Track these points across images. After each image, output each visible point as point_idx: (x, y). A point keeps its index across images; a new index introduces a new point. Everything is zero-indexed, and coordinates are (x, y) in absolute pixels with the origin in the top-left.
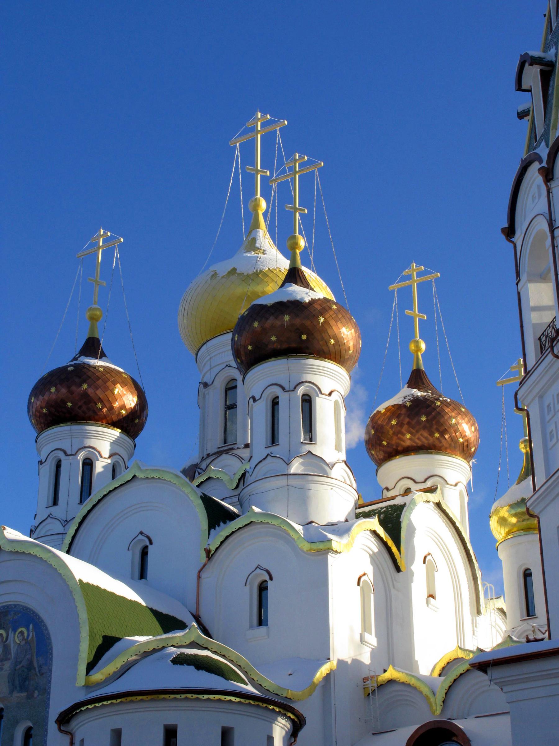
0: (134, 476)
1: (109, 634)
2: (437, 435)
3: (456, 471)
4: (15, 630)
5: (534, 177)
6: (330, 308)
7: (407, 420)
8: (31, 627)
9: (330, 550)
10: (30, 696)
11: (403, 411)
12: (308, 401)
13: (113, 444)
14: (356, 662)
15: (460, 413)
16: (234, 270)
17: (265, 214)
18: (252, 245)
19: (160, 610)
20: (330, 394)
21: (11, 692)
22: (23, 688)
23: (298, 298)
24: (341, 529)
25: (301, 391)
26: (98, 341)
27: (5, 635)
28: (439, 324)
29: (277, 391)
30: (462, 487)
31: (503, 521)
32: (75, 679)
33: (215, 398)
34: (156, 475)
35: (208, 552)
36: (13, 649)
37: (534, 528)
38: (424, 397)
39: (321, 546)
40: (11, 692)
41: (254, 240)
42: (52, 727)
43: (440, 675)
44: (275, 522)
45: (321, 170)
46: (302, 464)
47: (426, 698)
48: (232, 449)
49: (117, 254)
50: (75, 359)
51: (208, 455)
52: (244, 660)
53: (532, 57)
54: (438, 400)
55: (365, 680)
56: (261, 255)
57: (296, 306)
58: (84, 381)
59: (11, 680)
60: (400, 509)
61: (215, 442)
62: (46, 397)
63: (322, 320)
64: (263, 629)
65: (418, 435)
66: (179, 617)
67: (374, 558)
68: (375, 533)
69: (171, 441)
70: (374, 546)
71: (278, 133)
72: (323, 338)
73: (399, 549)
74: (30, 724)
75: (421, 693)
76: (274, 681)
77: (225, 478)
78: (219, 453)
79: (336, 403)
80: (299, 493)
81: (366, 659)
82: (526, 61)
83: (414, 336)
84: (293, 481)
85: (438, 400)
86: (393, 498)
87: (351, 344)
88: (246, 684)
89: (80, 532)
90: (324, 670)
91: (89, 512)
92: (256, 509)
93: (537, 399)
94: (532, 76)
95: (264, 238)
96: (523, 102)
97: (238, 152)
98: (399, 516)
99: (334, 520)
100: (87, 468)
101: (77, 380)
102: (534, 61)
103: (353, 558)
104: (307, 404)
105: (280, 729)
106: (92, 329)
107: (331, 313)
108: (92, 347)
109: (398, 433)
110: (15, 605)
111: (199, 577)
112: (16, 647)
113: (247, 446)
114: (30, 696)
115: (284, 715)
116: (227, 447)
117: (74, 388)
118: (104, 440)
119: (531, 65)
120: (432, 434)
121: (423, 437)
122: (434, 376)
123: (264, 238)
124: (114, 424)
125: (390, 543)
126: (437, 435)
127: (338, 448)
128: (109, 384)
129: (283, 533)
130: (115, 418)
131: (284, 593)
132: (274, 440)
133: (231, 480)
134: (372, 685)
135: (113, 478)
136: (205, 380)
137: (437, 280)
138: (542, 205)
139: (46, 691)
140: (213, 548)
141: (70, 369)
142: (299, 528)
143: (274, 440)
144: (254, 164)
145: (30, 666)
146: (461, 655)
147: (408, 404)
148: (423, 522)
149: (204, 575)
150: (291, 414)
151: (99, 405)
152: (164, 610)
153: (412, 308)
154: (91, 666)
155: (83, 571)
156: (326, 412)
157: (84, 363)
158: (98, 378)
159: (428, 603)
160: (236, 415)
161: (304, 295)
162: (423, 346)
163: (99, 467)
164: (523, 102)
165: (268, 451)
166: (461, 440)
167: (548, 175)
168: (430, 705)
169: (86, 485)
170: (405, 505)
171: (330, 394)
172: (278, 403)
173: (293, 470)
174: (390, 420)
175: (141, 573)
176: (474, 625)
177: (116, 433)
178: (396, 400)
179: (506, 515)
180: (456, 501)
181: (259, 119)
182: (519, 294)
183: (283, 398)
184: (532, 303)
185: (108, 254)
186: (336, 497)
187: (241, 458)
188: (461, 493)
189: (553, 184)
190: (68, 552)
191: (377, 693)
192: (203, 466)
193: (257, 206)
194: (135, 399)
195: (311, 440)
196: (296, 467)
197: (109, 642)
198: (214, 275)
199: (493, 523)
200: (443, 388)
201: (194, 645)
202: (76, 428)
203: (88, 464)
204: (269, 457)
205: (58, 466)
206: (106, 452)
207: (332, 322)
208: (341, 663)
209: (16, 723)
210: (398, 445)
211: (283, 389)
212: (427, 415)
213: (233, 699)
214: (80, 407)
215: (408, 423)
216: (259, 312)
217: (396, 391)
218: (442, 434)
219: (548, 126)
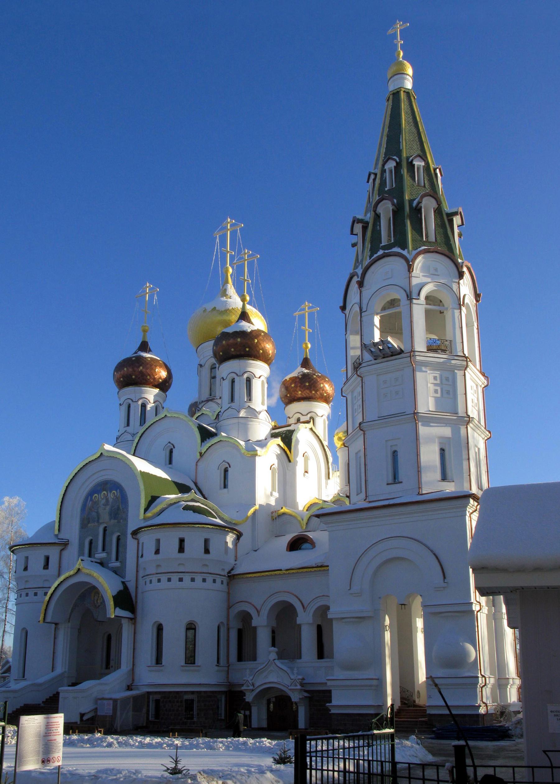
0: (166, 415)
1: (154, 495)
2: (313, 392)
3: (322, 410)
4: (111, 492)
5: (354, 286)
6: (260, 335)
7: (299, 385)
9: (256, 455)
10: (119, 522)
11: (298, 380)
12: (249, 381)
13: (155, 396)
14: (268, 505)
15: (325, 381)
16: (215, 308)
17: (231, 276)
18: (224, 293)
19: (178, 481)
20: (260, 377)
22: (115, 518)
23: (245, 329)
24: (262, 444)
25: (245, 376)
26: (147, 342)
28: (318, 334)
29: (234, 375)
30: (325, 417)
31: (340, 439)
32: (138, 515)
33: (206, 371)
34: (176, 415)
35: (201, 453)
36: (111, 500)
38: (308, 373)
39: (252, 453)
40: (110, 519)
41: (225, 290)
42: (129, 536)
43: (307, 510)
44: (231, 441)
45: (258, 260)
46: (245, 412)
47: (299, 522)
48: (214, 399)
49: (156, 297)
50: (136, 353)
51: (202, 402)
52: (216, 507)
53: (358, 219)
54: (315, 375)
55: (272, 513)
56: (229, 300)
57: (243, 334)
58: (141, 365)
59: (110, 514)
60: (292, 432)
61: (205, 395)
62: (122, 372)
63: (256, 341)
64: (226, 490)
65: (305, 392)
66: (188, 484)
67: (278, 456)
68: (279, 445)
69: (186, 390)
70: (278, 451)
71: (239, 231)
72: (257, 350)
73: (290, 451)
74: (119, 534)
75: (297, 519)
76: (231, 515)
77: (210, 414)
78: (207, 401)
79: (263, 382)
80: (244, 426)
81: (273, 503)
82: (355, 221)
83: (305, 340)
84: (241, 421)
85: (315, 375)
86: (289, 426)
87: (271, 352)
88: (216, 518)
89: (140, 441)
90: (252, 511)
91: (144, 431)
92: (223, 434)
93: (350, 393)
94: (358, 228)
95: (231, 290)
96: (354, 239)
97: (218, 240)
98: (291, 435)
99: (260, 439)
100: (143, 408)
101: (137, 365)
102: (359, 221)
103: (267, 458)
104: (248, 382)
105: (230, 538)
106: (144, 336)
107: (261, 337)
108: (144, 347)
109: (295, 391)
110: (111, 481)
111: (197, 465)
113: (220, 398)
114: (119, 522)
115: (233, 533)
116: (211, 399)
117: (135, 369)
118: (151, 394)
119: (358, 223)
120: (311, 392)
121: (307, 393)
122: (314, 362)
123: (231, 290)
124: (156, 386)
125: (286, 449)
126: (313, 392)
127: (263, 404)
128: (153, 366)
129: (236, 446)
130: (156, 383)
131: (235, 473)
132: (232, 400)
133: (213, 415)
134: (275, 515)
135: (156, 415)
136: (201, 363)
137: (318, 312)
138: (357, 299)
139: (126, 520)
140: (203, 452)
141: (134, 359)
142: (242, 443)
143: (232, 400)
144: (226, 248)
145: (118, 509)
146: (317, 501)
147: (300, 377)
148: (303, 436)
149: (199, 464)
150: (240, 387)
151: (148, 377)
152: (180, 481)
153: (304, 326)
154: (146, 510)
155: (142, 465)
156: (258, 387)
157: (140, 356)
158: (148, 364)
159: (304, 475)
160: (215, 381)
161: (247, 328)
162: (309, 346)
163: (149, 407)
164: (354, 239)
165: (229, 405)
166: (325, 394)
167: (361, 284)
168: (301, 525)
169: (143, 416)
170: (294, 431)
171: (260, 377)
172: (234, 382)
173: (241, 416)
174: (291, 384)
175: (169, 461)
176: (327, 484)
177: (157, 391)
178: (294, 374)
179: (341, 436)
180: (321, 427)
181: (228, 223)
182: (346, 340)
183: (237, 379)
184: (351, 346)
185: (151, 297)
186: (262, 427)
187: (218, 404)
188: (324, 420)
189: (363, 289)
190: (134, 455)
191: (277, 518)
192: (200, 406)
193: (227, 271)
194: (166, 373)
195: (250, 400)
196: (242, 414)
197: (153, 499)
198: (205, 311)
199: (336, 439)
200: (319, 366)
201: (193, 500)
202: (137, 388)
203: (144, 406)
204: (230, 409)
205: (129, 406)
206: (152, 401)
207: (261, 342)
208: (260, 505)
209: (112, 534)
210: (295, 396)
211: (237, 375)
212: (309, 383)
213: (209, 526)
214: (139, 378)
215: (300, 386)
216: (225, 335)
217: (296, 368)
218: (316, 391)
219: (363, 256)
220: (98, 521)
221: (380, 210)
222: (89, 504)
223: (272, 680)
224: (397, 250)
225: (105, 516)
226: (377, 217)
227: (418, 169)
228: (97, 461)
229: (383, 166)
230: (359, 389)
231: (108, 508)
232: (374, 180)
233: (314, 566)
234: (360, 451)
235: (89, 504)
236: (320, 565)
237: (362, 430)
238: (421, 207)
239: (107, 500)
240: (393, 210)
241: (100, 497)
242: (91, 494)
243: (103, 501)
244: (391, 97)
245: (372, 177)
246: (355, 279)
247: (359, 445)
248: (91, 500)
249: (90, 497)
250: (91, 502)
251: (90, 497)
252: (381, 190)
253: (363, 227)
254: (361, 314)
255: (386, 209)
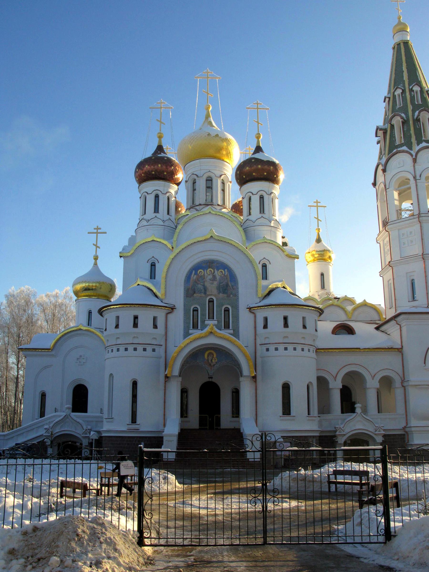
4: (218, 270)
8: (226, 270)
21: (219, 293)
27: (213, 271)
36: (218, 277)
37: (35, 488)
40: (219, 293)
59: (218, 288)
82: (378, 129)
94: (380, 133)
100: (157, 198)
102: (381, 129)
110: (217, 261)
112: (219, 277)
114: (228, 296)
117: (168, 167)
139: (236, 295)
145: (227, 285)
167: (384, 171)
220: (205, 293)
221: (394, 122)
222: (194, 277)
223: (358, 427)
224: (405, 148)
225: (212, 288)
226: (392, 126)
227: (417, 92)
228: (204, 242)
229: (394, 93)
230: (387, 239)
231: (215, 283)
232: (389, 101)
233: (387, 348)
234: (390, 280)
235: (194, 277)
236: (390, 347)
237: (391, 266)
238: (420, 118)
239: (214, 277)
240: (402, 122)
241: (208, 273)
242: (196, 268)
243: (211, 277)
244: (396, 46)
245: (387, 99)
246: (380, 167)
247: (389, 275)
248: (196, 273)
249: (194, 272)
250: (195, 276)
251: (194, 272)
252: (394, 110)
253: (383, 132)
254: (386, 190)
255: (397, 121)
